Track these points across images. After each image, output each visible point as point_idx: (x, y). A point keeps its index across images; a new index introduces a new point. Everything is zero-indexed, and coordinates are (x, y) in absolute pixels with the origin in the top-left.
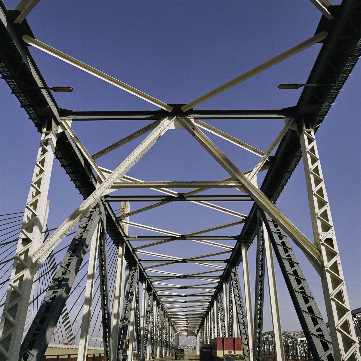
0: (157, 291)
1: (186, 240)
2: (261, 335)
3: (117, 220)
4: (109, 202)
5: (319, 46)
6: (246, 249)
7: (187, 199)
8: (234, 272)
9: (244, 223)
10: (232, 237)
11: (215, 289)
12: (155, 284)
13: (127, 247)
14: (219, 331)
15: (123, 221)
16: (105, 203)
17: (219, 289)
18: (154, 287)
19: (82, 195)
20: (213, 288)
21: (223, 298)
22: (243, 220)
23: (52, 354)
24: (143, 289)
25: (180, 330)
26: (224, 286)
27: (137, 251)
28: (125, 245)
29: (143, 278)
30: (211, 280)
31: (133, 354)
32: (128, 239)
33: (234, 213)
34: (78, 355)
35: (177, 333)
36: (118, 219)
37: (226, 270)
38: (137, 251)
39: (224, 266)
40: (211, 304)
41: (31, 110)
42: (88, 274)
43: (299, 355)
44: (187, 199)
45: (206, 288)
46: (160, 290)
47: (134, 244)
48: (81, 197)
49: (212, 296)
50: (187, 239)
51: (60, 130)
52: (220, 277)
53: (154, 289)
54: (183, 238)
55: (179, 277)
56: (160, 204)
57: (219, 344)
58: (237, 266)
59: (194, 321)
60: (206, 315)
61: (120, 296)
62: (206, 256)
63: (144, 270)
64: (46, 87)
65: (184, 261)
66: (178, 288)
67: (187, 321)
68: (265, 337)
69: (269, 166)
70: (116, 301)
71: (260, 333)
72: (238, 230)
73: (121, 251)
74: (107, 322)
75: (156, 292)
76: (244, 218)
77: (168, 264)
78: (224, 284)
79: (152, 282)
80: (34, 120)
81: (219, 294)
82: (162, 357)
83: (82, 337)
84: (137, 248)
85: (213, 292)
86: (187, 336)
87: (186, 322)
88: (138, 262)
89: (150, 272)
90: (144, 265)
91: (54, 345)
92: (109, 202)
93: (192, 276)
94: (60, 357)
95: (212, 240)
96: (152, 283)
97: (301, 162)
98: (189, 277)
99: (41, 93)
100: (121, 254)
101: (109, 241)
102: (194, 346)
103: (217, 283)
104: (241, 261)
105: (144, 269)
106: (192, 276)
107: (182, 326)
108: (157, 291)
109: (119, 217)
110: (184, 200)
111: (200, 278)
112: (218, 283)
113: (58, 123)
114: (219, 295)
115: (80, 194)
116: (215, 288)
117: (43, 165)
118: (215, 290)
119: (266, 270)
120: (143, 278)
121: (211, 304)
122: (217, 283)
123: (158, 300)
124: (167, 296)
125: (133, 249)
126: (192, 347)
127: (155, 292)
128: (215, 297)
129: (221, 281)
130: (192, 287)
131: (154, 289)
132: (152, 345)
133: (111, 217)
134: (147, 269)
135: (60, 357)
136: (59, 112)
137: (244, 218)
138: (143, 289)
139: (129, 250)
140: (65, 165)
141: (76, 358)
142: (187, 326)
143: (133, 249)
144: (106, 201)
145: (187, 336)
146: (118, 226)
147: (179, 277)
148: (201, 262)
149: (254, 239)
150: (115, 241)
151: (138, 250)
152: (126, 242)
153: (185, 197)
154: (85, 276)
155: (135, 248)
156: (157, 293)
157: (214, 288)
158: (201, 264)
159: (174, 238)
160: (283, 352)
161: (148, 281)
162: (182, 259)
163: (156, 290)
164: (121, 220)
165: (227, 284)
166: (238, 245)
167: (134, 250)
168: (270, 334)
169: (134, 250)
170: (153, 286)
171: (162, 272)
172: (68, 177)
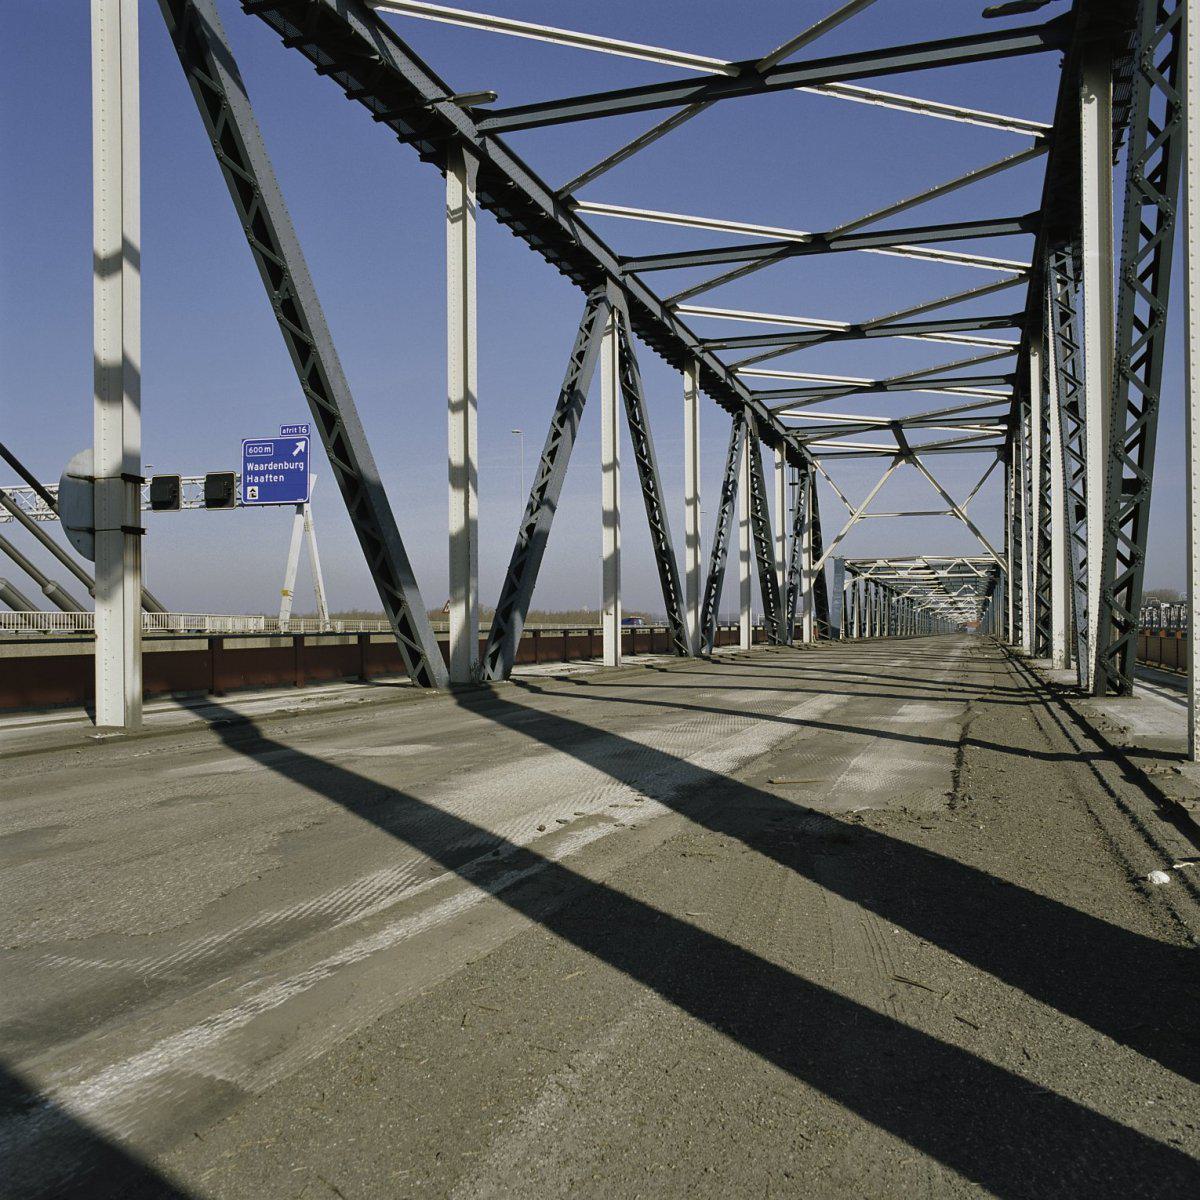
0: (777, 410)
1: (865, 337)
4: (500, 136)
9: (1046, 155)
14: (1050, 576)
15: (681, 307)
19: (525, 239)
20: (998, 381)
21: (1079, 311)
27: (738, 371)
28: (697, 365)
29: (768, 433)
31: (752, 629)
32: (629, 266)
33: (994, 264)
34: (448, 632)
36: (667, 306)
38: (738, 371)
46: (818, 435)
47: (662, 284)
48: (432, 169)
54: (818, 243)
55: (861, 389)
56: (692, 112)
63: (672, 316)
65: (856, 332)
76: (1024, 272)
77: (802, 345)
78: (1085, 90)
79: (777, 410)
81: (1053, 258)
85: (1003, 402)
93: (904, 383)
94: (306, 644)
98: (893, 387)
103: (1011, 353)
105: (772, 413)
106: (904, 383)
109: (561, 192)
111: (950, 426)
112: (1025, 286)
113: (812, 464)
117: (589, 331)
120: (768, 433)
122: (1011, 353)
124: (831, 430)
125: (662, 304)
133: (642, 306)
135: (228, 644)
137: (1024, 272)
146: (732, 383)
147: (861, 389)
148: (920, 328)
151: (740, 369)
155: (667, 301)
157: (1002, 380)
158: (944, 392)
167: (668, 308)
172: (538, 257)
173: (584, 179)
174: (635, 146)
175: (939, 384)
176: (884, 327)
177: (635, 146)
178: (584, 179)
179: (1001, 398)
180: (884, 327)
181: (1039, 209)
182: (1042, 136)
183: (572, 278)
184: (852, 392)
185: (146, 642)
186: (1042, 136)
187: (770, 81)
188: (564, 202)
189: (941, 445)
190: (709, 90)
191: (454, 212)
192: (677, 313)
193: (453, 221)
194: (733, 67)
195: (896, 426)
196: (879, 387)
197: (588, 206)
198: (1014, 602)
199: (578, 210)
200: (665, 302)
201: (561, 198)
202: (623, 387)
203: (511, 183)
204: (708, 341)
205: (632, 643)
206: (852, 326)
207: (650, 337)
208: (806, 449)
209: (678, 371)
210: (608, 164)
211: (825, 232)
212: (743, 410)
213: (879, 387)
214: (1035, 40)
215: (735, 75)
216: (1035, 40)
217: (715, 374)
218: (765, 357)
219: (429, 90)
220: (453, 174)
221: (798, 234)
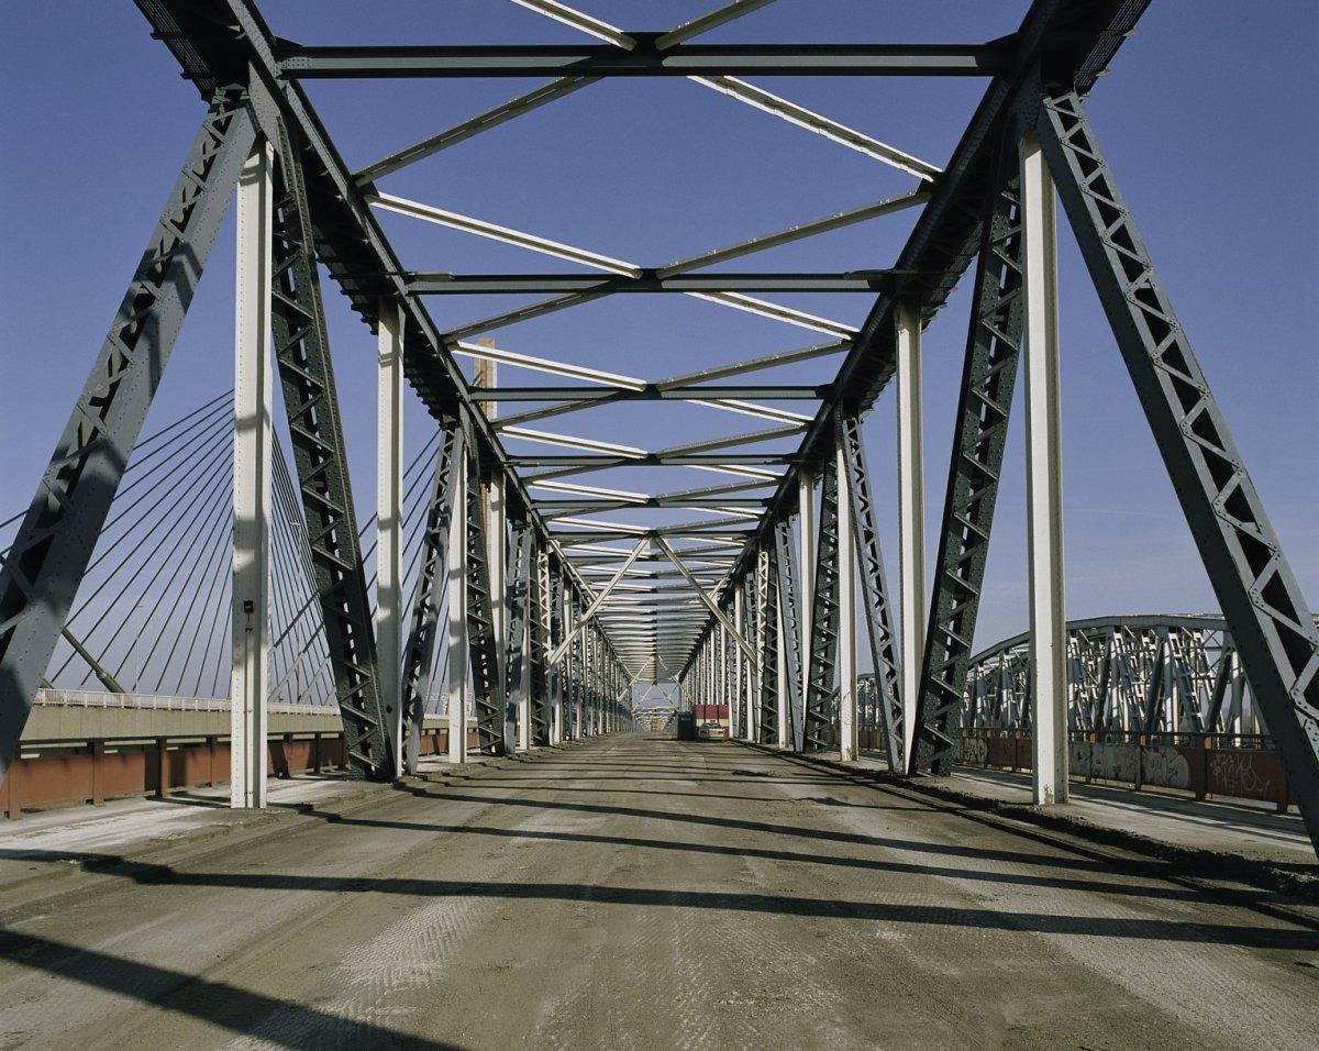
1: (660, 464)
2: (959, 661)
3: (355, 186)
4: (420, 296)
5: (922, 207)
6: (917, 329)
7: (665, 285)
8: (752, 582)
10: (858, 275)
11: (764, 506)
12: (541, 489)
13: (412, 323)
15: (461, 344)
16: (280, 84)
17: (782, 507)
18: (533, 502)
22: (920, 190)
23: (182, 734)
24: (494, 506)
25: (614, 592)
26: (803, 493)
30: (727, 541)
35: (590, 612)
36: (446, 341)
37: (815, 433)
39: (808, 411)
40: (748, 563)
41: (185, 45)
42: (239, 416)
43: (1126, 729)
44: (665, 285)
45: (729, 503)
46: (562, 511)
47: (444, 313)
49: (748, 533)
50: (663, 395)
51: (551, 550)
52: (787, 459)
53: (535, 509)
54: (649, 280)
56: (560, 90)
57: (700, 712)
58: (793, 514)
59: (674, 631)
60: (705, 637)
61: (260, 416)
62: (739, 368)
63: (492, 434)
64: (400, 271)
66: (622, 504)
67: (653, 655)
68: (1006, 657)
69: (929, 196)
70: (384, 538)
71: (957, 649)
72: (885, 244)
73: (385, 340)
74: (346, 610)
75: (542, 519)
76: (848, 338)
80: (200, 80)
82: (548, 745)
83: (238, 662)
84: (456, 332)
86: (655, 683)
87: (645, 548)
88: (467, 397)
89: (516, 439)
90: (493, 411)
91: (170, 700)
92: (420, 296)
93: (683, 456)
95: (748, 398)
96: (499, 434)
97: (889, 388)
98: (668, 461)
99: (324, 174)
100: (390, 351)
101: (334, 302)
102: (673, 707)
103: (796, 431)
104: (894, 371)
106: (683, 456)
107: (618, 570)
108: (530, 480)
110: (659, 397)
111: (707, 508)
114: (778, 533)
115: (363, 321)
116: (766, 502)
118: (781, 471)
119: (1023, 386)
120: (487, 464)
121: (748, 563)
123: (574, 588)
125: (440, 338)
126: (667, 710)
127: (537, 519)
128: (764, 537)
129: (792, 474)
130: (683, 500)
131: (535, 509)
132: (479, 680)
134: (505, 428)
135: (323, 736)
136: (271, 46)
137: (848, 338)
138: (494, 506)
139: (425, 339)
140: (197, 70)
141: (229, 744)
142: (654, 646)
143: (440, 338)
144: (286, 74)
145: (655, 683)
146: (364, 222)
148: (714, 393)
149: (963, 270)
150: (422, 389)
152: (407, 299)
153: (660, 277)
154: (369, 524)
156: (529, 488)
159: (624, 394)
160: (1062, 723)
161: (508, 476)
162: (645, 382)
163: (541, 512)
164: (371, 191)
165: (817, 483)
166: (881, 315)
167: (447, 342)
168: (867, 680)
169: (446, 341)
170: (528, 497)
171: (503, 230)
173: (394, 163)
174: (475, 126)
175: (715, 460)
176: (684, 388)
177: (475, 126)
178: (394, 163)
179: (751, 517)
180: (684, 388)
181: (892, 265)
182: (931, 180)
183: (331, 270)
184: (621, 507)
185: (226, 733)
186: (931, 180)
187: (668, 62)
188: (363, 190)
189: (692, 528)
190: (596, 62)
191: (384, 357)
192: (455, 352)
193: (383, 365)
194: (626, 37)
195: (653, 535)
196: (652, 459)
197: (390, 203)
198: (810, 681)
199: (456, 352)
200: (522, 479)
201: (360, 184)
202: (285, 372)
203: (340, 197)
204: (537, 501)
205: (281, 755)
206: (651, 499)
207: (423, 386)
208: (525, 491)
209: (368, 327)
210: (433, 145)
211: (657, 267)
212: (246, 82)
213: (652, 459)
214: (970, 61)
215: (629, 48)
216: (970, 61)
217: (425, 336)
218: (514, 317)
219: (390, 267)
220: (324, 265)
221: (627, 267)
